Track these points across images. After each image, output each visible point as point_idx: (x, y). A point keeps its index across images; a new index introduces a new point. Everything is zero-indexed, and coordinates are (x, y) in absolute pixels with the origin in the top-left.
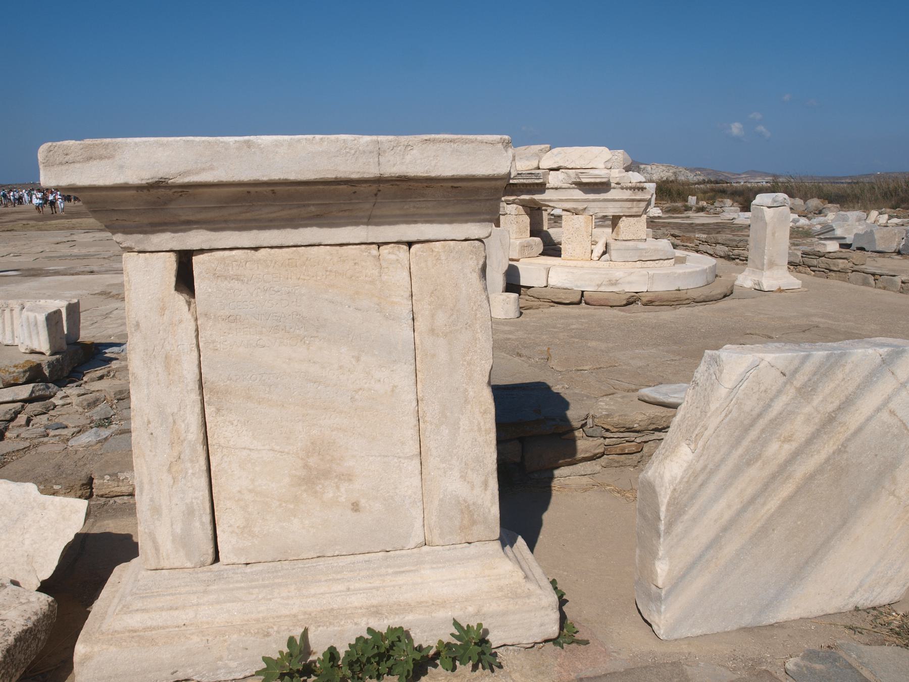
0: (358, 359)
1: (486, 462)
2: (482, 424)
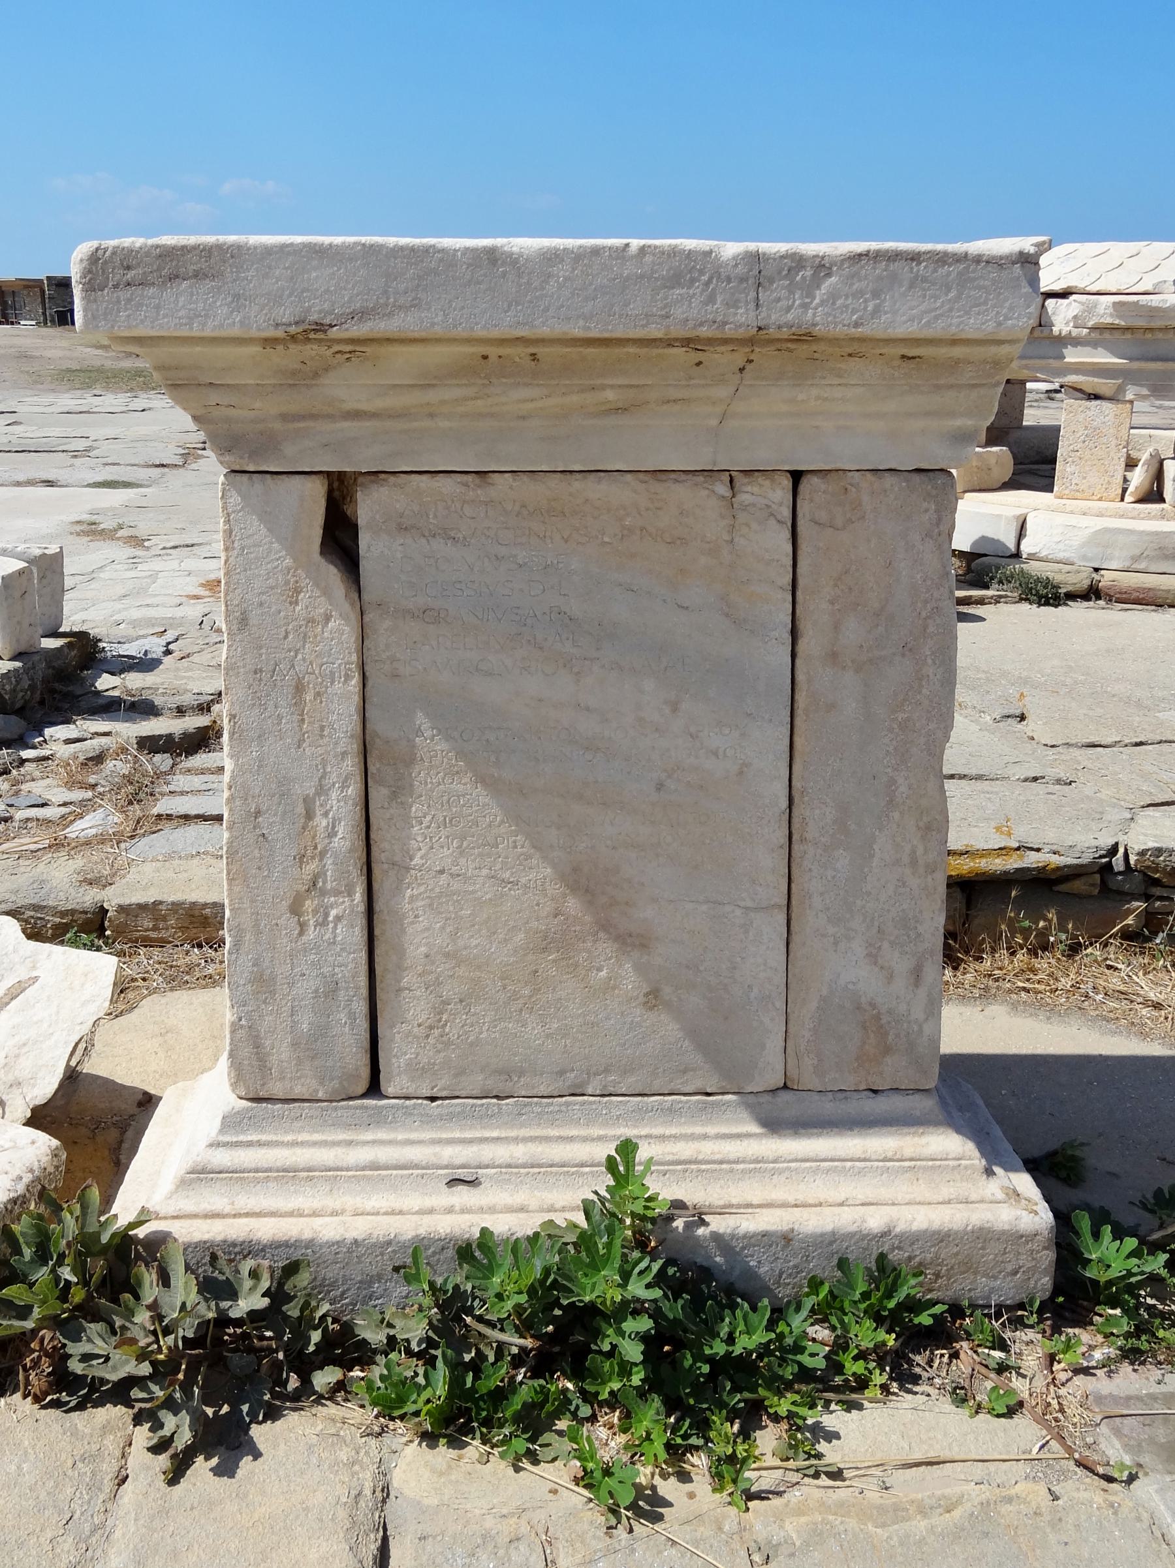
0: (675, 708)
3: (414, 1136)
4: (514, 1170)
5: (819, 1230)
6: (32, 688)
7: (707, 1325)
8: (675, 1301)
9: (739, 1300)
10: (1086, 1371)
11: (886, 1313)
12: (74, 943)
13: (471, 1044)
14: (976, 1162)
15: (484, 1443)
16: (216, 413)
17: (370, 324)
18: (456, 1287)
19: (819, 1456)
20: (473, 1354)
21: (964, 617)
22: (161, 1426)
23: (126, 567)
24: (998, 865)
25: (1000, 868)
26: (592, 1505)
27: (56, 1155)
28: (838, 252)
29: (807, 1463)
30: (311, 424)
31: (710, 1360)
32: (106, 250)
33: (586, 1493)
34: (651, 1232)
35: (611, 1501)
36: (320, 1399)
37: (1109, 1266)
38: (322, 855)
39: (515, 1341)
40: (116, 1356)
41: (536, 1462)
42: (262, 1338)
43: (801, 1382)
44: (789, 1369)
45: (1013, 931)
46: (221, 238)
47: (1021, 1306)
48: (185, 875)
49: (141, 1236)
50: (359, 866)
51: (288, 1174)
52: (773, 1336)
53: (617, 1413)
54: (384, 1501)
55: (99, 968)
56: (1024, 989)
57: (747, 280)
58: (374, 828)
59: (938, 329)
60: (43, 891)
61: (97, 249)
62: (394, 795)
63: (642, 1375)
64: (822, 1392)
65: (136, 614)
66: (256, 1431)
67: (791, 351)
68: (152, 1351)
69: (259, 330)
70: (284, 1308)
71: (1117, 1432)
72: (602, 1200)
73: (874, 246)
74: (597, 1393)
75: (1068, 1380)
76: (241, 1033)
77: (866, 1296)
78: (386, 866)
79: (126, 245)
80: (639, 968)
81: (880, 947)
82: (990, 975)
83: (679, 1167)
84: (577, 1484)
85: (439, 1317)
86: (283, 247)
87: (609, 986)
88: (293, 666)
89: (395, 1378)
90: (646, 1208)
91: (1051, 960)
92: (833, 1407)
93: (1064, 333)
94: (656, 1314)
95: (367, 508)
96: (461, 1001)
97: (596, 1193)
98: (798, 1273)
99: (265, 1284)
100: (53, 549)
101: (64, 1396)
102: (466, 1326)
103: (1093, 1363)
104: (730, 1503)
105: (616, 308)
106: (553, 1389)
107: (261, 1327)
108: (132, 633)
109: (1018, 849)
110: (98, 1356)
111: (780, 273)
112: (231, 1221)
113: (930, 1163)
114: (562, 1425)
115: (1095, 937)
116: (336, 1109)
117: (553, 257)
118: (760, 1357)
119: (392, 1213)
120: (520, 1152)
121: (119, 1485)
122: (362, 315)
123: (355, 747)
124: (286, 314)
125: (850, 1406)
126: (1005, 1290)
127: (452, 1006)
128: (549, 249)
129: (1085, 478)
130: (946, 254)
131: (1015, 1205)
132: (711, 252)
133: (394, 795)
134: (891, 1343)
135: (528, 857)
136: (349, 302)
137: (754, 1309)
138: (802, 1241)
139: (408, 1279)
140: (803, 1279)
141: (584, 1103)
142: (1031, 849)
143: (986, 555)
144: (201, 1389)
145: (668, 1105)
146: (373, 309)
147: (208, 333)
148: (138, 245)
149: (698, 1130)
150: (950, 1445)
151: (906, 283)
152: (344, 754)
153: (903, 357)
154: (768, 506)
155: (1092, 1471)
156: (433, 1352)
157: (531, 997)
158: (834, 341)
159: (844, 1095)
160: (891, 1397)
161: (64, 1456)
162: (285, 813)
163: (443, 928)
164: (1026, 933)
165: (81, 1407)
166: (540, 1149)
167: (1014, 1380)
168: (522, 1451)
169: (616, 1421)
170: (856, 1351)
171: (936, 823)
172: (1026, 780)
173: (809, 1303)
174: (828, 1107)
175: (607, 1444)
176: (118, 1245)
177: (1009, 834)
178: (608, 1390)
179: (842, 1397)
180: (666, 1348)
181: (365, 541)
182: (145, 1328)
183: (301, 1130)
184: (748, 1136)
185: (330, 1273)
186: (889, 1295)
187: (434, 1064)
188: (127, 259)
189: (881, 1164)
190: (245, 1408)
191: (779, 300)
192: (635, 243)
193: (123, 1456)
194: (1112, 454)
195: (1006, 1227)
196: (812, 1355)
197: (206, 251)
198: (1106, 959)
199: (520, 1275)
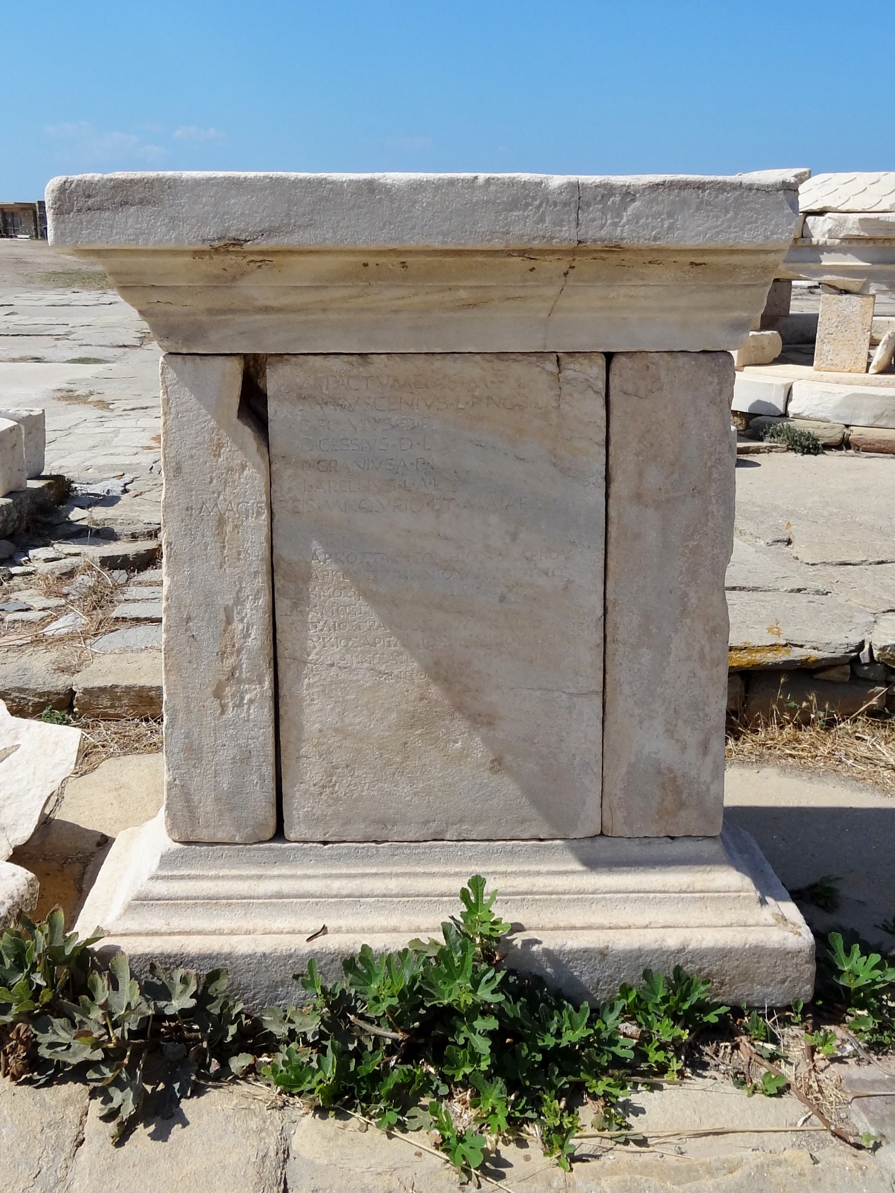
0: (514, 537)
1: (707, 710)
3: (310, 872)
5: (628, 948)
6: (20, 519)
7: (540, 1022)
8: (515, 1003)
9: (565, 1002)
10: (840, 1060)
11: (682, 1013)
12: (50, 719)
13: (356, 800)
14: (753, 894)
15: (364, 1116)
18: (343, 991)
19: (628, 1127)
20: (356, 1045)
21: (741, 463)
22: (111, 1100)
23: (95, 424)
24: (770, 658)
26: (448, 1165)
27: (31, 885)
28: (641, 183)
29: (619, 1133)
30: (230, 317)
31: (542, 1050)
32: (72, 182)
34: (496, 948)
36: (235, 1080)
37: (858, 976)
38: (239, 651)
39: (389, 1035)
40: (76, 1044)
41: (405, 1131)
42: (191, 1030)
43: (613, 1068)
44: (605, 1057)
45: (782, 710)
46: (161, 174)
47: (789, 1008)
48: (136, 665)
49: (97, 949)
50: (267, 660)
51: (211, 901)
52: (592, 1031)
53: (469, 1092)
54: (285, 1161)
56: (791, 755)
57: (570, 205)
58: (279, 631)
59: (719, 242)
61: (65, 182)
62: (295, 605)
63: (489, 1062)
66: (185, 1104)
67: (603, 259)
68: (104, 1041)
70: (208, 1007)
71: (865, 1109)
73: (669, 177)
74: (453, 1076)
77: (665, 999)
79: (87, 179)
82: (764, 745)
83: (518, 897)
84: (437, 1149)
85: (329, 1015)
86: (209, 179)
87: (463, 755)
88: (216, 504)
89: (294, 1063)
91: (812, 733)
92: (640, 1088)
94: (500, 1014)
95: (274, 382)
96: (347, 766)
97: (452, 918)
99: (193, 988)
100: (37, 412)
101: (36, 1075)
102: (350, 1022)
104: (557, 1165)
105: (467, 227)
106: (418, 1073)
108: (98, 476)
109: (786, 645)
110: (62, 1044)
111: (595, 199)
112: (168, 938)
113: (716, 895)
114: (425, 1101)
116: (249, 850)
117: (418, 187)
118: (582, 1048)
120: (393, 885)
121: (77, 1146)
124: (211, 231)
126: (775, 995)
127: (340, 770)
128: (415, 181)
129: (838, 355)
130: (725, 183)
131: (784, 928)
132: (542, 182)
133: (295, 605)
134: (685, 1037)
135: (400, 654)
137: (577, 1009)
139: (305, 985)
141: (444, 846)
142: (796, 646)
143: (760, 415)
147: (150, 246)
148: (96, 179)
149: (534, 868)
151: (694, 206)
153: (692, 263)
154: (587, 380)
155: (845, 1141)
156: (324, 1042)
158: (638, 251)
159: (648, 840)
160: (685, 1080)
161: (34, 1124)
162: (210, 619)
163: (333, 709)
164: (792, 711)
165: (48, 1084)
166: (409, 882)
167: (783, 1066)
168: (394, 1122)
169: (468, 1098)
170: (658, 1044)
171: (719, 626)
172: (792, 591)
173: (620, 1005)
174: (635, 850)
175: (461, 1117)
177: (779, 634)
178: (462, 1073)
179: (646, 1080)
180: (508, 1040)
181: (272, 407)
183: (223, 866)
184: (573, 872)
185: (245, 979)
186: (684, 999)
188: (87, 190)
189: (677, 895)
190: (177, 1086)
191: (594, 220)
192: (482, 176)
194: (859, 336)
195: (777, 946)
196: (623, 1047)
197: (149, 184)
198: (856, 732)
199: (392, 982)
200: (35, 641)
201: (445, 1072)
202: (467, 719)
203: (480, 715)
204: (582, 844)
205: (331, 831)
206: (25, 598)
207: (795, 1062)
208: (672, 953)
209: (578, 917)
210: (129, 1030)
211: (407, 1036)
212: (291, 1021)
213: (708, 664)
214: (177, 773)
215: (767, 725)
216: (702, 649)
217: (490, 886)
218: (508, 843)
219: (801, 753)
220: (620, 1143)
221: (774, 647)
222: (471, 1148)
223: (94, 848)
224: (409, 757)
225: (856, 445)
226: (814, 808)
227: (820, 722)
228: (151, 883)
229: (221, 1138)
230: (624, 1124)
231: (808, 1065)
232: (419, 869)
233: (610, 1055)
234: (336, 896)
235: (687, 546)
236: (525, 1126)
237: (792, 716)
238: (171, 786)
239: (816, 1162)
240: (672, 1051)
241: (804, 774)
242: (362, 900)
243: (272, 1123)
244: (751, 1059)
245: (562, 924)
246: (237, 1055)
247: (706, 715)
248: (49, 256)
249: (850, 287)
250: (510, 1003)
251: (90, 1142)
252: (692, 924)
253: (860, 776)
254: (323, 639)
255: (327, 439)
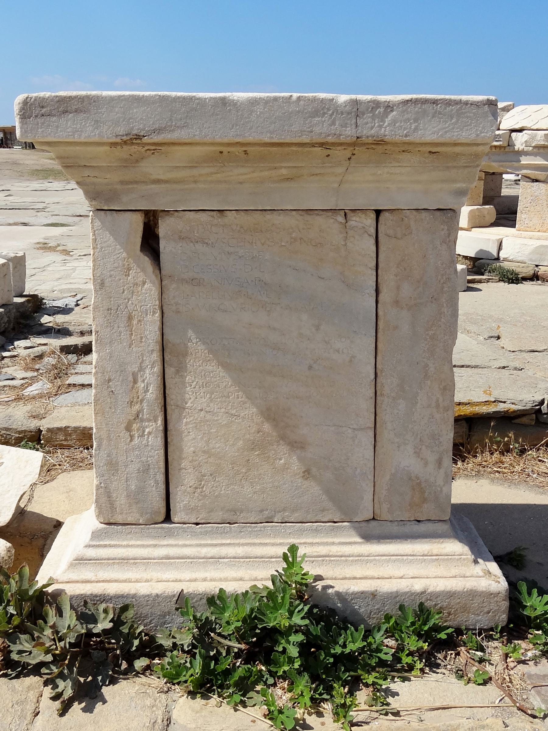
0: (318, 328)
1: (441, 440)
2: (441, 400)
3: (188, 542)
4: (237, 560)
5: (390, 591)
6: (9, 322)
7: (332, 638)
8: (317, 626)
9: (349, 625)
10: (524, 662)
11: (423, 632)
12: (25, 447)
13: (217, 496)
14: (470, 557)
15: (219, 697)
16: (88, 180)
17: (163, 135)
18: (207, 618)
19: (388, 704)
20: (215, 652)
21: (469, 289)
22: (57, 687)
23: (61, 264)
24: (485, 409)
25: (485, 411)
26: (272, 728)
27: (9, 551)
28: (397, 100)
29: (382, 708)
30: (135, 186)
31: (334, 656)
32: (31, 98)
33: (270, 722)
34: (305, 591)
35: (283, 727)
36: (137, 674)
37: (536, 609)
38: (142, 401)
39: (236, 646)
40: (35, 651)
41: (245, 706)
42: (110, 643)
43: (379, 667)
44: (374, 660)
45: (492, 443)
46: (89, 93)
47: (492, 629)
48: (81, 414)
49: (50, 591)
50: (160, 407)
51: (124, 561)
52: (365, 643)
53: (287, 682)
54: (168, 725)
55: (33, 458)
56: (497, 471)
57: (351, 113)
58: (167, 388)
59: (447, 138)
60: (11, 421)
61: (27, 98)
62: (178, 372)
63: (299, 663)
64: (390, 672)
65: (64, 287)
66: (104, 690)
67: (374, 149)
68: (52, 649)
69: (108, 138)
70: (121, 628)
71: (539, 693)
72: (280, 575)
73: (414, 96)
74: (277, 672)
75: (515, 667)
76: (102, 490)
77: (413, 624)
78: (173, 407)
79: (41, 96)
80: (300, 459)
81: (421, 449)
82: (481, 465)
83: (320, 559)
84: (265, 718)
85: (198, 633)
86: (120, 97)
87: (285, 468)
88: (127, 307)
89: (175, 664)
90: (302, 579)
91: (511, 457)
92: (396, 679)
93: (520, 150)
94: (307, 633)
95: (164, 229)
96: (211, 475)
97: (277, 571)
98: (379, 612)
99: (111, 616)
100: (20, 254)
101: (9, 672)
102: (212, 638)
103: (528, 658)
104: (342, 728)
105: (286, 128)
106: (254, 670)
107: (110, 638)
108: (60, 295)
109: (495, 402)
110: (26, 652)
111: (367, 110)
112: (95, 584)
113: (446, 557)
114: (258, 688)
115: (533, 446)
116: (148, 529)
117: (254, 102)
118: (360, 654)
119: (176, 581)
120: (240, 551)
121: (35, 716)
122: (159, 131)
123: (158, 347)
124: (121, 130)
125: (405, 679)
126: (483, 621)
127: (207, 477)
128: (252, 98)
129: (531, 221)
130: (450, 100)
131: (489, 578)
132: (333, 99)
133: (178, 372)
134: (426, 648)
135: (245, 403)
136: (152, 124)
137: (357, 630)
138: (381, 596)
139: (182, 614)
140: (382, 615)
141: (272, 527)
142: (501, 402)
143: (482, 259)
144: (77, 668)
145: (314, 528)
146: (165, 128)
147: (82, 140)
148: (47, 96)
149: (330, 540)
150: (454, 699)
151: (431, 115)
152: (152, 351)
153: (430, 152)
154: (364, 227)
155: (525, 713)
156: (194, 650)
157: (246, 473)
158: (395, 144)
159: (403, 523)
160: (425, 675)
161: (7, 702)
162: (123, 380)
163: (202, 438)
164: (498, 443)
165: (17, 677)
166: (250, 549)
167: (487, 666)
168: (238, 701)
169: (286, 686)
170: (408, 652)
171: (449, 387)
172: (499, 368)
173: (384, 627)
174: (395, 529)
175: (281, 698)
176: (37, 596)
177: (490, 395)
178: (282, 670)
179: (400, 675)
180: (313, 650)
181: (162, 244)
182: (49, 638)
183: (131, 539)
184: (355, 543)
185: (145, 611)
186: (425, 624)
187: (198, 506)
188: (42, 103)
189: (422, 557)
190: (100, 678)
191: (367, 123)
192: (295, 95)
193: (38, 702)
194: (544, 209)
195: (484, 590)
196: (386, 654)
197: (81, 99)
198: (539, 457)
199: (238, 612)
200: (17, 399)
201: (271, 669)
202: (288, 445)
203: (296, 442)
204: (361, 525)
205: (201, 516)
206: (11, 371)
207: (495, 663)
208: (418, 594)
209: (358, 571)
210: (69, 643)
211: (248, 647)
212: (174, 637)
213: (441, 410)
214: (102, 479)
215: (482, 452)
216: (438, 401)
217: (301, 552)
218: (314, 524)
219: (504, 470)
220: (382, 714)
221: (487, 403)
222: (287, 717)
223: (51, 529)
224: (250, 469)
225: (542, 278)
226: (511, 505)
227: (516, 450)
228: (86, 549)
229: (127, 711)
230: (385, 702)
231: (503, 665)
232: (258, 541)
233: (377, 659)
234: (203, 558)
235: (428, 334)
236: (322, 703)
237: (498, 447)
238: (98, 488)
239: (507, 726)
240: (417, 656)
241: (505, 483)
242: (220, 560)
243: (160, 701)
244: (467, 661)
245: (348, 576)
246: (139, 659)
247: (441, 442)
248: (33, 160)
249: (539, 178)
250: (314, 625)
251: (43, 713)
252: (430, 576)
253: (541, 485)
254: (196, 393)
255: (198, 265)
